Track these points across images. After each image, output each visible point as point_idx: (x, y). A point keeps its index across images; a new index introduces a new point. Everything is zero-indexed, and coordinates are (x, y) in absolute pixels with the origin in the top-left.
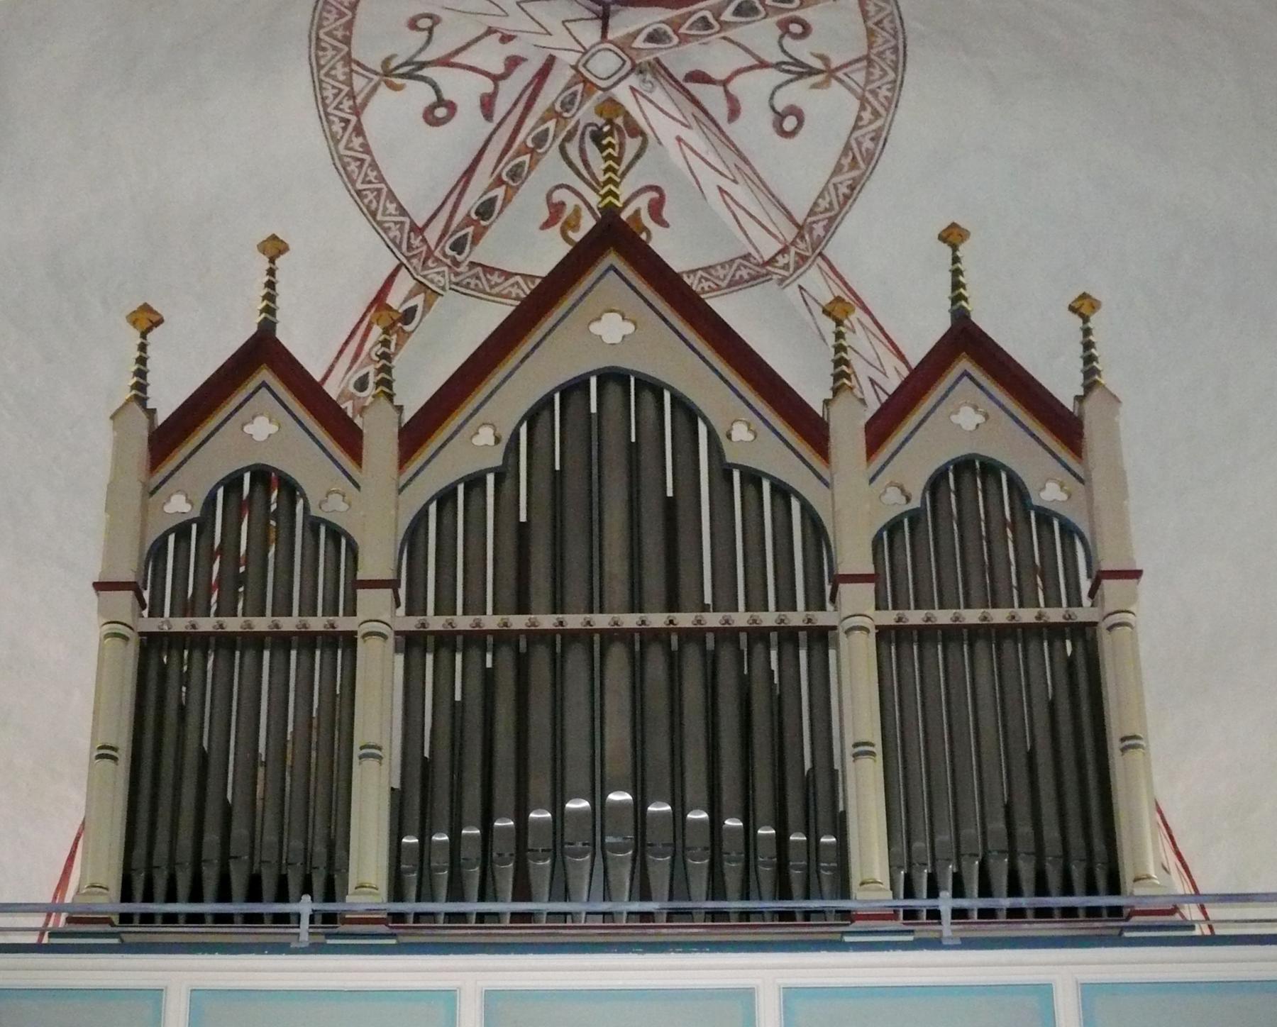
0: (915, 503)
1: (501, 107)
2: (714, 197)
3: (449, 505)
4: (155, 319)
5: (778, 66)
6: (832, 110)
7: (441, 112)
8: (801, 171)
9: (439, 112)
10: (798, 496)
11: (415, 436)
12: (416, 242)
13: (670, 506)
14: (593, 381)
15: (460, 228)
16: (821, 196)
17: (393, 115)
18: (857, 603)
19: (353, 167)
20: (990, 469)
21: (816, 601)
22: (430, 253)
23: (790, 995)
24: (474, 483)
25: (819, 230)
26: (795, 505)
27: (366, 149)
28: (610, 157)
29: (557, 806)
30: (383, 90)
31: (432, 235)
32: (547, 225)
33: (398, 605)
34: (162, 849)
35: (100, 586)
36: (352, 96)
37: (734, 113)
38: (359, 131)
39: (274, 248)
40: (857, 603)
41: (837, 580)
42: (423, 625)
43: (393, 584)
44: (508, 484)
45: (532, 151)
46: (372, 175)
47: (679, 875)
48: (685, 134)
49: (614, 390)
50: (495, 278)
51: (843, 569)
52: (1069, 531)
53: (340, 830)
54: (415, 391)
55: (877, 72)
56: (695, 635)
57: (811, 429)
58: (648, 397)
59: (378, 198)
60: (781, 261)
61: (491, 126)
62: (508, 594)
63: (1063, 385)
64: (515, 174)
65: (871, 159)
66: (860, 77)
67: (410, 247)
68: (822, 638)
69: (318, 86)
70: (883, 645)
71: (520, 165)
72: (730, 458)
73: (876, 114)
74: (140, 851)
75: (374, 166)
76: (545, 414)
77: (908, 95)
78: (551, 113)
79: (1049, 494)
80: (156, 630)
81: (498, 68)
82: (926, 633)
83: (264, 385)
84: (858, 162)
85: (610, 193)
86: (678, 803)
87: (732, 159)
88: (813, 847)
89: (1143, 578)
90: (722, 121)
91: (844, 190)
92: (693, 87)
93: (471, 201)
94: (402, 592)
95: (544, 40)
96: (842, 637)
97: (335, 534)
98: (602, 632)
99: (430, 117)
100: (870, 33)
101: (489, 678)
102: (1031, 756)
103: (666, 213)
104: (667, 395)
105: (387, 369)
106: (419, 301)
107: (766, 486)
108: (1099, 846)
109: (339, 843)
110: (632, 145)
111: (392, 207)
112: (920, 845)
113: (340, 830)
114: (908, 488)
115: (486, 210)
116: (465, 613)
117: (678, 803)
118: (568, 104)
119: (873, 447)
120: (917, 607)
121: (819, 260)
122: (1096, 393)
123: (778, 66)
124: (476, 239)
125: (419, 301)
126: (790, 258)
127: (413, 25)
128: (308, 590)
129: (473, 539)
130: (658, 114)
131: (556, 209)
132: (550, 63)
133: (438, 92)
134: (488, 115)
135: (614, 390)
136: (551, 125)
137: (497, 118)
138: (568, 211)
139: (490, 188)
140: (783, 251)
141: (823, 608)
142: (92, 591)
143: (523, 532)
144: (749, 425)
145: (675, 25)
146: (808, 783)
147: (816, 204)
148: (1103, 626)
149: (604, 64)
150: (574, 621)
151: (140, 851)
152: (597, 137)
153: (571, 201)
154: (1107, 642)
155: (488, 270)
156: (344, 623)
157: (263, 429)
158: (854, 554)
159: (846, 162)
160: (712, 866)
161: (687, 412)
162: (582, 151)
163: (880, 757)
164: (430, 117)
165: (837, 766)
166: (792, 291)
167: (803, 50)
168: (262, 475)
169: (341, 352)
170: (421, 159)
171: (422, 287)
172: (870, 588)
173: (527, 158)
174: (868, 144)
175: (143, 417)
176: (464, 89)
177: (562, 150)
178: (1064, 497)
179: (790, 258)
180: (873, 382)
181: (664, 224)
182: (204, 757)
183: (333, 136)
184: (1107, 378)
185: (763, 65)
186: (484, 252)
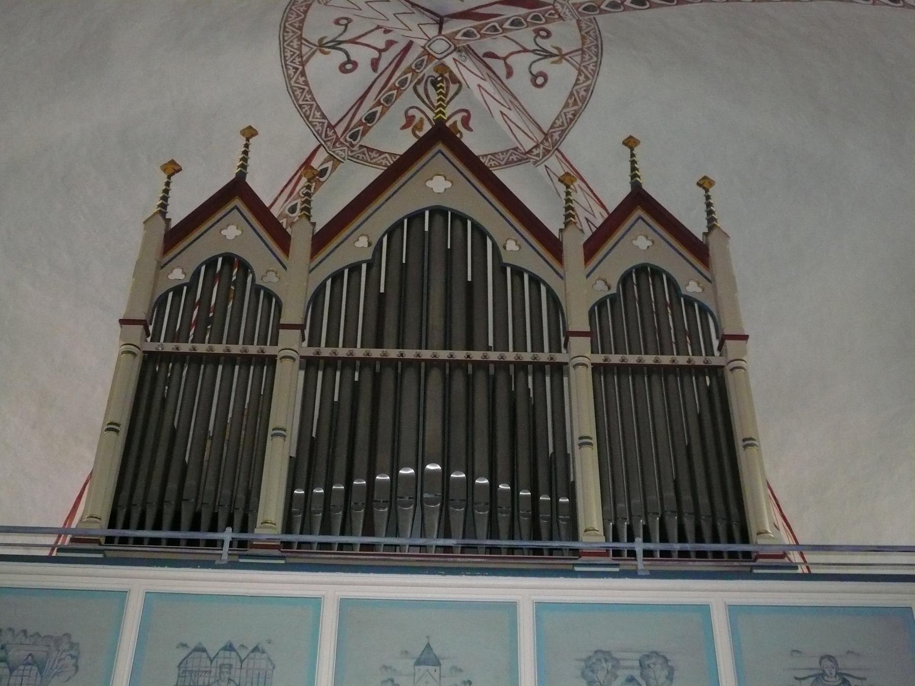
0: (614, 291)
1: (382, 65)
2: (498, 117)
4: (177, 168)
5: (533, 51)
6: (563, 75)
7: (349, 66)
8: (547, 105)
12: (330, 133)
14: (427, 213)
15: (355, 127)
16: (557, 118)
17: (322, 68)
18: (580, 347)
19: (298, 92)
20: (656, 272)
21: (556, 347)
22: (338, 139)
24: (354, 269)
26: (543, 289)
27: (306, 83)
28: (441, 93)
30: (318, 54)
31: (340, 130)
32: (404, 127)
34: (139, 492)
35: (123, 322)
36: (301, 56)
37: (510, 73)
38: (303, 74)
40: (580, 347)
41: (568, 334)
42: (318, 353)
43: (302, 327)
45: (398, 88)
46: (308, 97)
48: (482, 83)
49: (439, 219)
50: (373, 154)
51: (572, 328)
52: (704, 310)
54: (323, 215)
55: (587, 57)
56: (483, 365)
57: (552, 246)
59: (311, 109)
60: (535, 152)
63: (698, 228)
64: (388, 100)
65: (585, 101)
66: (578, 59)
67: (326, 136)
68: (559, 369)
69: (283, 50)
71: (391, 95)
72: (505, 261)
73: (587, 78)
74: (125, 494)
75: (310, 92)
77: (604, 69)
78: (409, 70)
79: (692, 288)
81: (382, 46)
84: (577, 102)
86: (470, 472)
87: (508, 97)
88: (554, 505)
90: (503, 78)
93: (363, 113)
95: (408, 33)
96: (572, 370)
97: (269, 295)
99: (343, 69)
100: (583, 38)
102: (688, 449)
103: (471, 124)
104: (469, 223)
105: (308, 202)
106: (329, 165)
107: (526, 277)
108: (734, 510)
109: (254, 492)
110: (453, 88)
111: (318, 114)
115: (371, 118)
117: (470, 472)
118: (419, 66)
119: (588, 256)
121: (556, 152)
122: (715, 231)
123: (533, 51)
125: (329, 165)
126: (540, 150)
127: (337, 22)
130: (469, 74)
131: (410, 119)
133: (348, 56)
135: (439, 219)
136: (409, 75)
137: (380, 71)
139: (374, 106)
140: (536, 147)
141: (560, 351)
142: (118, 325)
145: (479, 29)
146: (551, 462)
147: (554, 123)
148: (728, 368)
150: (410, 354)
151: (125, 494)
152: (434, 83)
153: (418, 115)
154: (730, 378)
155: (370, 150)
157: (233, 233)
158: (578, 320)
159: (571, 101)
161: (481, 233)
162: (426, 90)
164: (343, 69)
165: (569, 451)
166: (541, 169)
167: (547, 44)
169: (282, 191)
172: (587, 340)
173: (395, 92)
174: (582, 93)
176: (363, 55)
178: (700, 290)
179: (540, 150)
180: (587, 220)
181: (470, 129)
182: (174, 432)
183: (288, 76)
184: (722, 223)
185: (525, 50)
186: (367, 141)
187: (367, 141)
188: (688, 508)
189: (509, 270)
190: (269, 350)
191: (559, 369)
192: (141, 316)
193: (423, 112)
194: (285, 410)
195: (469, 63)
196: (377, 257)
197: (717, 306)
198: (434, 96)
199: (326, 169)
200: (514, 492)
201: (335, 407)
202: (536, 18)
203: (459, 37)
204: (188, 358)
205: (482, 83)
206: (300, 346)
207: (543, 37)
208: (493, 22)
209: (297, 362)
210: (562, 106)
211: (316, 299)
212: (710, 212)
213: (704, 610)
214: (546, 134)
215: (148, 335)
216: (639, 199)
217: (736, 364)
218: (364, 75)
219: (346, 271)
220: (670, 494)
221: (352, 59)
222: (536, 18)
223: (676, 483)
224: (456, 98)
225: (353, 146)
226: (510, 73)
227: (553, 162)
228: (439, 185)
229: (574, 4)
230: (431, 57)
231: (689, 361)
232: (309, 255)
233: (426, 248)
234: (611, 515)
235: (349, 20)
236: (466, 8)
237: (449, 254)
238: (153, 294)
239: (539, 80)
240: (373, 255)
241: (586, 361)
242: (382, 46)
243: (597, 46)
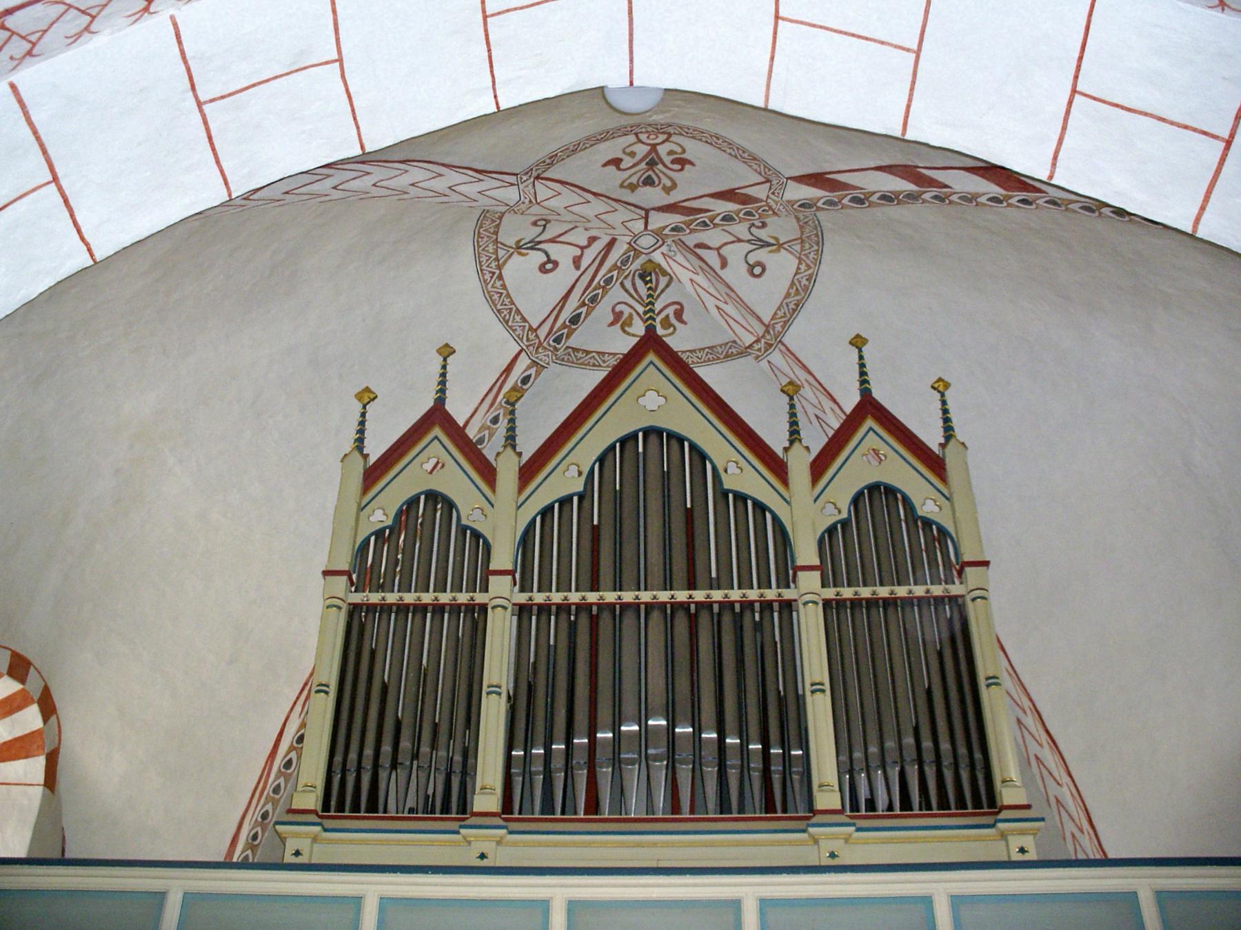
0: (844, 515)
1: (585, 263)
2: (714, 311)
3: (549, 515)
4: (372, 396)
5: (748, 241)
6: (782, 266)
7: (549, 266)
8: (764, 296)
9: (548, 267)
10: (771, 512)
11: (528, 472)
12: (532, 337)
13: (689, 514)
14: (640, 434)
15: (559, 330)
16: (779, 309)
17: (520, 271)
18: (809, 582)
19: (496, 297)
20: (891, 491)
21: (785, 582)
22: (540, 344)
23: (765, 905)
24: (565, 502)
25: (778, 327)
26: (768, 516)
27: (504, 287)
28: (649, 289)
29: (615, 728)
30: (515, 256)
31: (542, 333)
32: (612, 324)
33: (515, 584)
34: (353, 756)
35: (326, 573)
36: (497, 259)
37: (724, 264)
38: (500, 277)
39: (447, 351)
40: (809, 582)
41: (797, 569)
42: (530, 599)
43: (511, 573)
44: (586, 504)
45: (603, 287)
46: (507, 301)
47: (698, 781)
48: (694, 277)
49: (653, 439)
50: (580, 355)
51: (800, 562)
52: (943, 532)
53: (472, 744)
54: (529, 444)
55: (807, 246)
56: (707, 606)
57: (777, 467)
58: (674, 444)
59: (510, 313)
60: (756, 347)
61: (579, 273)
62: (586, 578)
63: (932, 437)
64: (594, 299)
65: (808, 290)
66: (798, 248)
67: (528, 340)
68: (788, 606)
69: (477, 256)
70: (829, 612)
71: (597, 295)
72: (727, 485)
73: (809, 267)
74: (338, 758)
75: (508, 296)
76: (610, 456)
77: (826, 257)
78: (615, 267)
79: (928, 508)
80: (359, 601)
81: (584, 243)
83: (436, 437)
84: (799, 294)
85: (651, 318)
86: (697, 725)
87: (724, 289)
88: (786, 758)
89: (991, 565)
90: (717, 269)
91: (792, 306)
92: (698, 251)
93: (566, 315)
94: (518, 576)
95: (611, 231)
96: (801, 606)
97: (477, 535)
98: (646, 604)
99: (543, 269)
100: (801, 227)
101: (573, 627)
102: (929, 692)
103: (685, 317)
104: (686, 444)
105: (512, 412)
106: (533, 371)
107: (750, 503)
108: (978, 756)
109: (471, 753)
110: (663, 281)
111: (518, 318)
112: (858, 755)
113: (472, 744)
114: (839, 505)
115: (575, 320)
116: (558, 591)
117: (697, 725)
118: (624, 262)
120: (849, 585)
121: (780, 345)
122: (952, 442)
123: (748, 241)
124: (568, 336)
125: (533, 371)
126: (762, 345)
127: (535, 224)
128: (457, 575)
129: (564, 529)
130: (681, 268)
131: (617, 316)
132: (612, 242)
133: (548, 256)
134: (577, 267)
135: (653, 439)
136: (615, 273)
137: (582, 269)
138: (626, 315)
139: (578, 308)
140: (758, 341)
141: (788, 587)
142: (321, 576)
143: (596, 530)
144: (736, 463)
145: (688, 224)
146: (782, 702)
147: (776, 313)
148: (968, 598)
149: (646, 241)
150: (628, 597)
151: (338, 758)
152: (642, 277)
153: (627, 311)
154: (974, 612)
155: (575, 350)
158: (806, 552)
159: (793, 291)
160: (720, 770)
161: (700, 456)
162: (634, 285)
163: (828, 692)
164: (543, 269)
165: (800, 692)
166: (764, 364)
167: (763, 234)
168: (433, 497)
169: (483, 400)
170: (536, 293)
171: (534, 363)
172: (817, 574)
173: (600, 291)
174: (804, 282)
175: (361, 460)
176: (563, 254)
177: (622, 284)
178: (937, 509)
179: (762, 345)
180: (817, 417)
181: (684, 322)
182: (385, 688)
183: (485, 281)
184: (959, 433)
185: (739, 240)
186: (573, 341)
187: (573, 341)
188: (928, 757)
189: (731, 496)
190: (480, 598)
191: (788, 606)
192: (345, 566)
193: (631, 307)
194: (498, 666)
195: (679, 258)
196: (589, 487)
197: (956, 527)
198: (643, 289)
199: (529, 376)
200: (745, 742)
201: (552, 651)
202: (749, 213)
203: (666, 231)
204: (394, 608)
205: (694, 277)
206: (512, 591)
207: (758, 227)
208: (703, 217)
209: (510, 609)
210: (783, 296)
211: (525, 541)
212: (947, 420)
213: (927, 902)
214: (767, 326)
215: (352, 584)
216: (869, 407)
217: (977, 593)
218: (565, 275)
219: (557, 505)
220: (909, 740)
221: (553, 258)
222: (749, 213)
223: (916, 730)
224: (667, 290)
225: (555, 348)
226: (724, 264)
227: (776, 357)
228: (652, 401)
229: (789, 202)
230: (638, 253)
231: (928, 591)
232: (516, 489)
233: (642, 538)
234: (847, 769)
235: (548, 221)
236: (672, 202)
237: (665, 477)
238: (355, 542)
239: (756, 270)
240: (586, 484)
241: (814, 597)
242: (584, 243)
243: (817, 235)
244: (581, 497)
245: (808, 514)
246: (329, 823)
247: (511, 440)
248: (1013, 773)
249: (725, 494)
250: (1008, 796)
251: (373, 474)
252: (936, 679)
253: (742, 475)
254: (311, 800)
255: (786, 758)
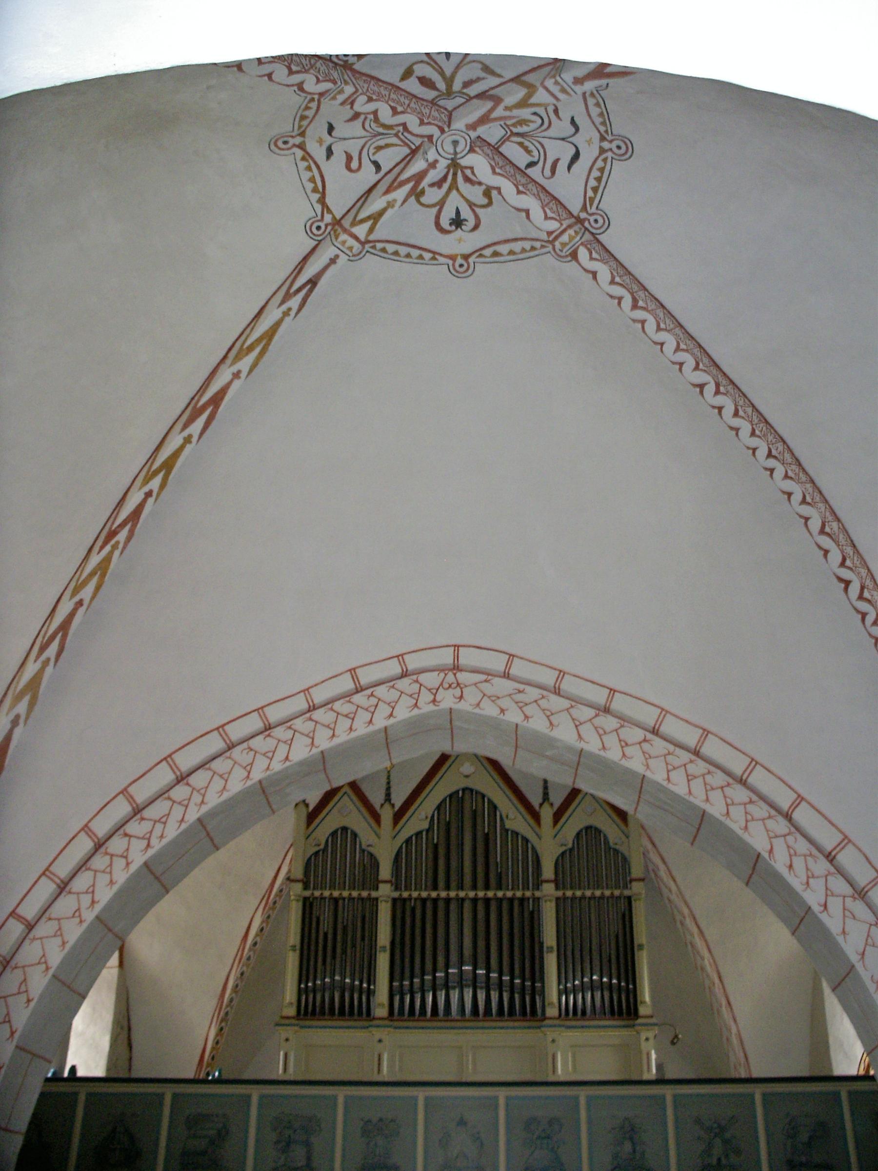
11: (398, 816)
18: (548, 889)
20: (598, 831)
24: (418, 834)
26: (530, 845)
40: (548, 889)
43: (390, 882)
44: (430, 833)
54: (398, 800)
68: (537, 900)
72: (507, 827)
76: (443, 805)
82: (571, 884)
83: (345, 793)
119: (556, 822)
156: (374, 894)
157: (346, 814)
158: (548, 872)
161: (494, 807)
191: (537, 900)
219: (414, 838)
244: (428, 831)
245: (550, 844)
246: (302, 1023)
247: (388, 797)
248: (647, 998)
249: (507, 830)
250: (642, 1011)
251: (312, 817)
252: (613, 952)
253: (515, 819)
254: (292, 1011)
255: (533, 986)
